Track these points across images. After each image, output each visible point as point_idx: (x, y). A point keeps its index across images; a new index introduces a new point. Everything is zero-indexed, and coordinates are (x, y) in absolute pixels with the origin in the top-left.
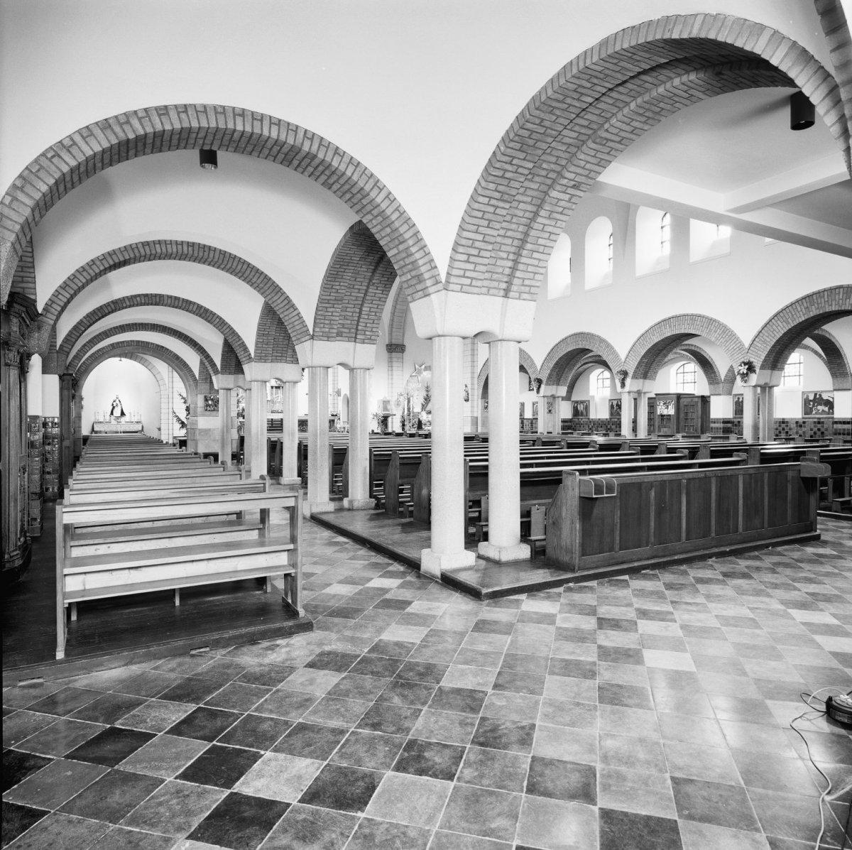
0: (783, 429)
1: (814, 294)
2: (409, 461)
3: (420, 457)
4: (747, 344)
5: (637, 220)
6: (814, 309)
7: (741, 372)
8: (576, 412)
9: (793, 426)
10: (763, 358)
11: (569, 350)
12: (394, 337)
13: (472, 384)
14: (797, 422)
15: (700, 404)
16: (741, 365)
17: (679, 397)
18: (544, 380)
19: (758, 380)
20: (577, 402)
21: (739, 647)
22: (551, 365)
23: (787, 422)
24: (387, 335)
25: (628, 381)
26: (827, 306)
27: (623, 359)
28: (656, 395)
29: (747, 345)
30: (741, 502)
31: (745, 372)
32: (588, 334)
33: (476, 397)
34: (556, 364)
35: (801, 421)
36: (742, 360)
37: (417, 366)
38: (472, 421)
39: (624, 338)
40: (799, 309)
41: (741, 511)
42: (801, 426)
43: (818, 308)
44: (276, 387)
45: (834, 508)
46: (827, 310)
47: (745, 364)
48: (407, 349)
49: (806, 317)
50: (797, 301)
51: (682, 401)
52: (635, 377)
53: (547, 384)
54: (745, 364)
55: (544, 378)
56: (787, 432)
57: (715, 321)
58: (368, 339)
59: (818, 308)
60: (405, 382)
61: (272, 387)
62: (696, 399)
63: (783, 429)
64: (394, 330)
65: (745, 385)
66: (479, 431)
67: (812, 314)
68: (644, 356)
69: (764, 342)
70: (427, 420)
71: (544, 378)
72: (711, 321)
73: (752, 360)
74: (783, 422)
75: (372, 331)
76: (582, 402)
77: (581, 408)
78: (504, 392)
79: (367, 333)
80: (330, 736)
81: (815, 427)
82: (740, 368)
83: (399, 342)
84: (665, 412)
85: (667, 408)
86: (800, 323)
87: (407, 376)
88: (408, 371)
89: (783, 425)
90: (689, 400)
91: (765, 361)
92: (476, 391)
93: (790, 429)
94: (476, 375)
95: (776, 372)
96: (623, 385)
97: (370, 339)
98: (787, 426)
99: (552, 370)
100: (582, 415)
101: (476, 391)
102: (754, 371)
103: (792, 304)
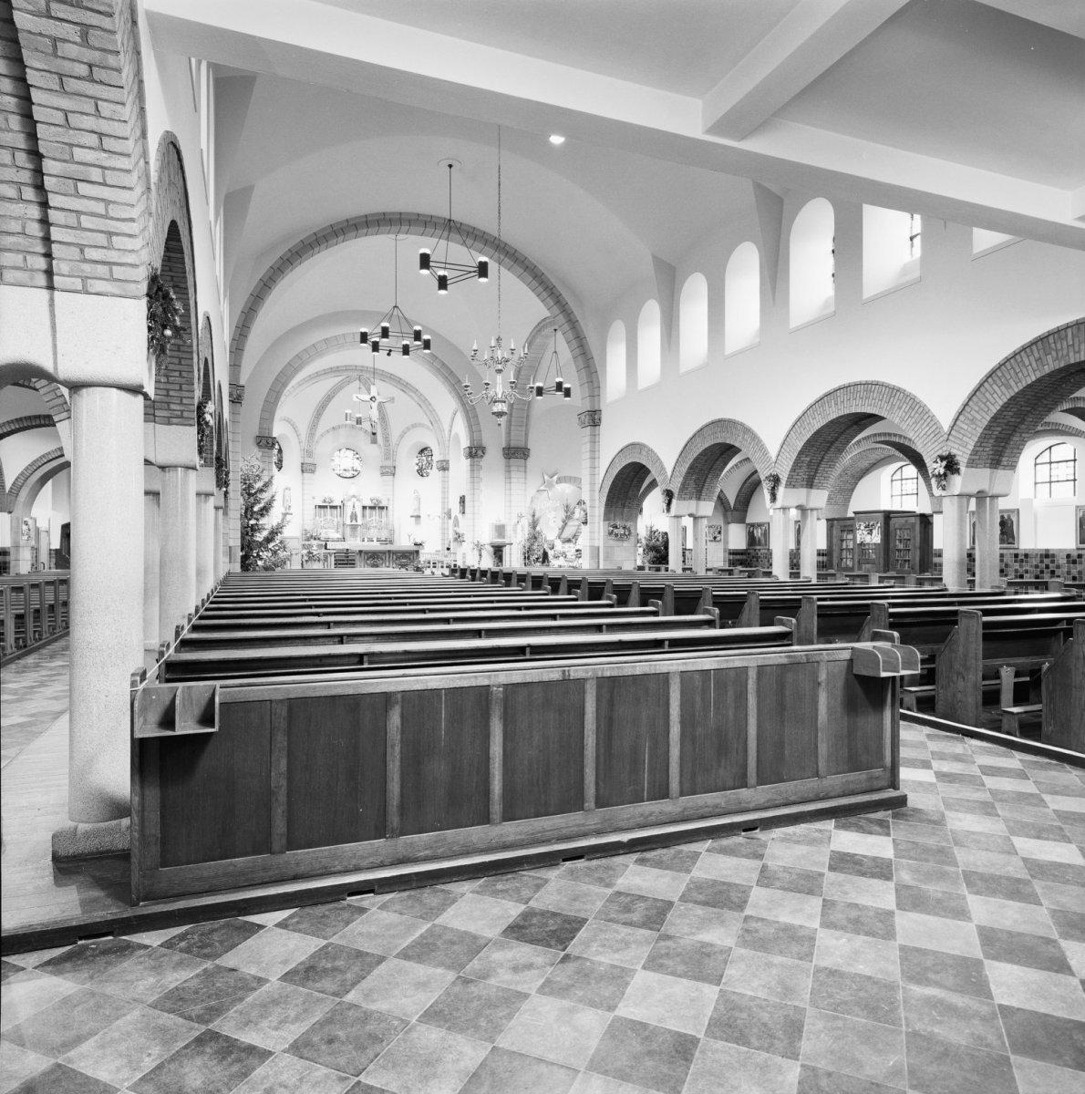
0: (1047, 567)
1: (1050, 334)
2: (788, 605)
3: (800, 600)
4: (946, 423)
5: (791, 238)
6: (1050, 361)
7: (936, 472)
8: (752, 540)
9: (1063, 561)
10: (971, 448)
11: (707, 445)
12: (512, 438)
13: (592, 500)
14: (1068, 556)
15: (918, 528)
16: (936, 462)
17: (888, 515)
18: (676, 492)
19: (963, 484)
20: (752, 525)
21: (989, 937)
22: (684, 468)
23: (1053, 556)
24: (504, 435)
25: (781, 491)
26: (1071, 354)
27: (774, 459)
28: (855, 513)
29: (946, 428)
30: (675, 730)
31: (942, 472)
32: (730, 421)
33: (597, 519)
34: (691, 468)
35: (1075, 554)
36: (939, 453)
37: (546, 477)
38: (592, 552)
39: (774, 428)
40: (1027, 363)
41: (675, 752)
42: (1074, 562)
43: (1057, 358)
44: (371, 508)
45: (1005, 726)
46: (1072, 361)
47: (942, 458)
48: (532, 453)
49: (1039, 375)
50: (1024, 349)
51: (893, 521)
52: (790, 484)
53: (680, 498)
54: (942, 458)
55: (675, 488)
56: (1053, 572)
57: (899, 390)
58: (177, 417)
59: (1057, 358)
60: (529, 500)
61: (364, 508)
62: (912, 520)
63: (1047, 567)
64: (512, 428)
65: (944, 493)
66: (601, 567)
67: (1047, 370)
68: (801, 453)
69: (973, 421)
70: (562, 550)
71: (675, 488)
72: (895, 391)
73: (954, 452)
74: (1047, 556)
75: (181, 403)
76: (760, 525)
77: (758, 533)
78: (988, 523)
79: (173, 407)
80: (341, 1034)
81: (1042, 562)
82: (935, 465)
83: (522, 444)
84: (868, 539)
85: (870, 533)
86: (1029, 386)
87: (532, 491)
88: (534, 483)
89: (1047, 561)
90: (903, 520)
91: (975, 452)
92: (597, 510)
93: (1058, 567)
94: (597, 487)
95: (1000, 473)
96: (774, 497)
97: (182, 417)
98: (1053, 562)
99: (686, 478)
100: (760, 544)
101: (597, 510)
102: (957, 471)
103: (1015, 354)
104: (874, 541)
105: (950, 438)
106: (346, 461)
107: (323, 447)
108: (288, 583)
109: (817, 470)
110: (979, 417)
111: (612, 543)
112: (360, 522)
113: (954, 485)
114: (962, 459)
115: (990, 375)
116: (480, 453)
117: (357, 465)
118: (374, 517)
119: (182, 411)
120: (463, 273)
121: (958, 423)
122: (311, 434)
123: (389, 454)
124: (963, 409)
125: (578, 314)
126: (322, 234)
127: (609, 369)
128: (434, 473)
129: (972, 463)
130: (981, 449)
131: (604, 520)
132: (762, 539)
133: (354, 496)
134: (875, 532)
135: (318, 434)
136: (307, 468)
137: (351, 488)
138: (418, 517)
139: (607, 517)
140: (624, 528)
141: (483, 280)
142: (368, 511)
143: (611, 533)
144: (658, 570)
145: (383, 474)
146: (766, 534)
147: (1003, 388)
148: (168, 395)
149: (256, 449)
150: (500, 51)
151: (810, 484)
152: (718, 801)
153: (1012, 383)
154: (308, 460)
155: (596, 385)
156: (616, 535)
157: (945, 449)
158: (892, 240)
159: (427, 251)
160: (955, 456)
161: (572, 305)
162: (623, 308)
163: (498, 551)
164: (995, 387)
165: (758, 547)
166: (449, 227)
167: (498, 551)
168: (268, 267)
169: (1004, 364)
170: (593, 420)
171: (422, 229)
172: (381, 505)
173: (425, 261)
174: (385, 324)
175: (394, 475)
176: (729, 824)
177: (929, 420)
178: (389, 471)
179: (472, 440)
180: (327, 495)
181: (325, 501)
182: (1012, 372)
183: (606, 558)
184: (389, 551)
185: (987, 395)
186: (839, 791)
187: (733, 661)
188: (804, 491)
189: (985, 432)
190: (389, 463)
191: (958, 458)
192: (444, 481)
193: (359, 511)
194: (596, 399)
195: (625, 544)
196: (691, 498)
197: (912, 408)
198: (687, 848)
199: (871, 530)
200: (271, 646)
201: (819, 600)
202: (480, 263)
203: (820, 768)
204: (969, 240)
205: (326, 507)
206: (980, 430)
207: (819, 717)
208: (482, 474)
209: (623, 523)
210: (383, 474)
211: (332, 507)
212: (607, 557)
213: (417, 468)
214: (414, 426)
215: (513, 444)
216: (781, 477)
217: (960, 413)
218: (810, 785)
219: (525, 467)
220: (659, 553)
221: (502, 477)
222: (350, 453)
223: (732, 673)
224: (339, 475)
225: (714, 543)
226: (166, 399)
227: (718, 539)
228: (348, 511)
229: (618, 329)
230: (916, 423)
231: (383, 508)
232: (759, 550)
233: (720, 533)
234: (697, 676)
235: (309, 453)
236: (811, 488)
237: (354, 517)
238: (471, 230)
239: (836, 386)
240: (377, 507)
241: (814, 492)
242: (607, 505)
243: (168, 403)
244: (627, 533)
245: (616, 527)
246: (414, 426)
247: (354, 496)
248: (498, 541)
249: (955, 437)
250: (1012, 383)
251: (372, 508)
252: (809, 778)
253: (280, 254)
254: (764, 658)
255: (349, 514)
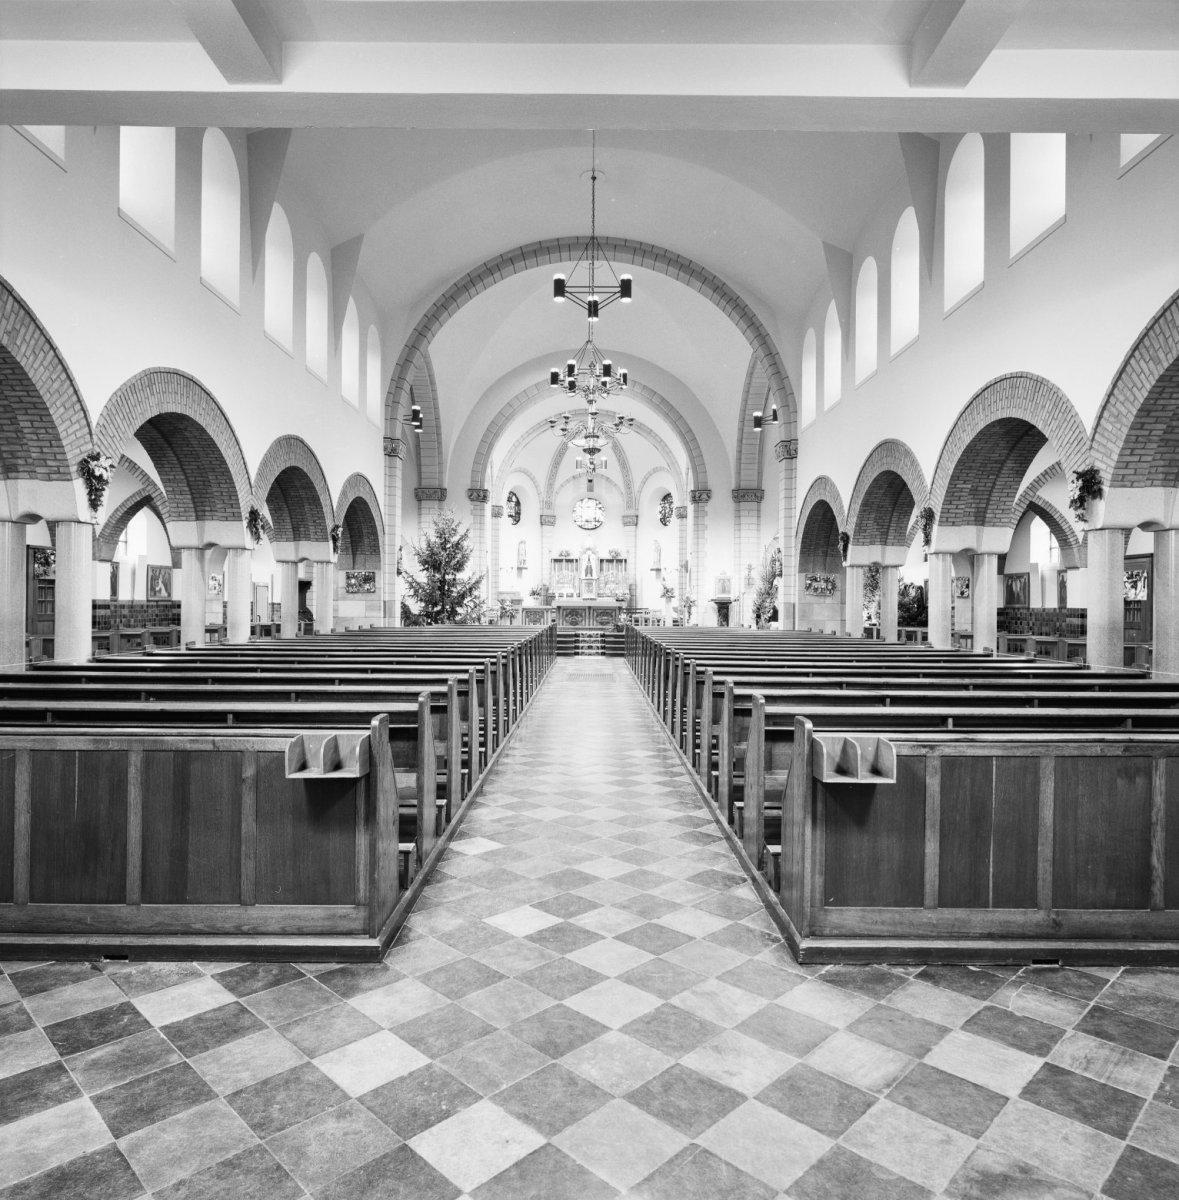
10: (1115, 457)
12: (742, 478)
13: (788, 547)
25: (936, 529)
44: (608, 561)
53: (857, 543)
61: (602, 561)
75: (56, 459)
76: (1019, 576)
77: (1017, 587)
79: (50, 463)
83: (754, 485)
85: (1134, 586)
104: (1139, 598)
105: (1095, 445)
106: (588, 511)
107: (564, 498)
108: (438, 639)
109: (989, 500)
110: (1124, 411)
111: (811, 599)
112: (595, 576)
113: (1097, 514)
114: (1106, 476)
115: (1136, 348)
116: (704, 496)
117: (599, 515)
118: (611, 571)
119: (58, 467)
120: (609, 295)
121: (1103, 421)
122: (550, 485)
123: (631, 501)
124: (1108, 401)
125: (768, 327)
126: (475, 275)
127: (804, 393)
128: (674, 520)
129: (1120, 481)
130: (1136, 459)
131: (800, 572)
132: (1021, 594)
133: (589, 549)
134: (1140, 584)
135: (557, 485)
136: (547, 520)
137: (589, 539)
138: (658, 570)
139: (803, 568)
140: (827, 581)
141: (626, 300)
142: (605, 564)
143: (808, 587)
144: (910, 637)
145: (625, 524)
146: (1026, 587)
147: (1151, 364)
148: (42, 452)
149: (467, 502)
150: (29, 43)
151: (980, 519)
152: (81, 915)
153: (1162, 355)
154: (549, 512)
155: (791, 409)
156: (816, 590)
157: (1087, 462)
158: (1042, 166)
159: (561, 276)
160: (1097, 471)
161: (762, 317)
162: (807, 319)
163: (723, 608)
164: (1142, 363)
165: (1017, 606)
166: (592, 246)
167: (723, 608)
168: (422, 316)
169: (1152, 327)
170: (789, 452)
171: (630, 256)
172: (620, 558)
173: (560, 288)
174: (572, 362)
175: (636, 525)
176: (83, 946)
177: (1072, 421)
178: (632, 521)
179: (696, 482)
180: (565, 548)
181: (561, 555)
182: (1161, 338)
183: (803, 617)
184: (590, 608)
185: (1134, 376)
186: (276, 927)
187: (107, 742)
188: (972, 530)
189: (1134, 432)
190: (632, 512)
191: (1102, 474)
192: (681, 530)
193: (595, 565)
194: (792, 425)
195: (829, 600)
196: (872, 543)
197: (1056, 405)
198: (156, 966)
199: (1135, 582)
200: (393, 701)
201: (715, 673)
202: (623, 281)
203: (243, 891)
204: (1115, 149)
205: (561, 561)
206: (1125, 430)
207: (243, 825)
208: (707, 521)
209: (824, 575)
210: (625, 524)
211: (568, 561)
212: (803, 616)
213: (660, 516)
214: (655, 470)
215: (743, 485)
216: (934, 510)
217: (1104, 408)
218: (1016, 917)
219: (759, 511)
220: (914, 612)
221: (754, 527)
222: (592, 503)
223: (107, 757)
224: (581, 527)
225: (962, 600)
226: (42, 456)
227: (966, 594)
228: (583, 565)
229: (810, 336)
230: (1059, 427)
231: (621, 561)
232: (1019, 609)
233: (967, 586)
234: (55, 757)
235: (549, 505)
236: (983, 525)
237: (589, 571)
238: (638, 246)
239: (982, 384)
240: (616, 560)
241: (988, 531)
242: (802, 552)
243: (45, 460)
244: (830, 587)
245: (816, 580)
246: (655, 470)
247: (589, 549)
248: (724, 596)
249: (1100, 444)
250: (1162, 355)
251: (610, 561)
252: (227, 903)
253: (434, 300)
254: (155, 741)
255: (584, 567)
